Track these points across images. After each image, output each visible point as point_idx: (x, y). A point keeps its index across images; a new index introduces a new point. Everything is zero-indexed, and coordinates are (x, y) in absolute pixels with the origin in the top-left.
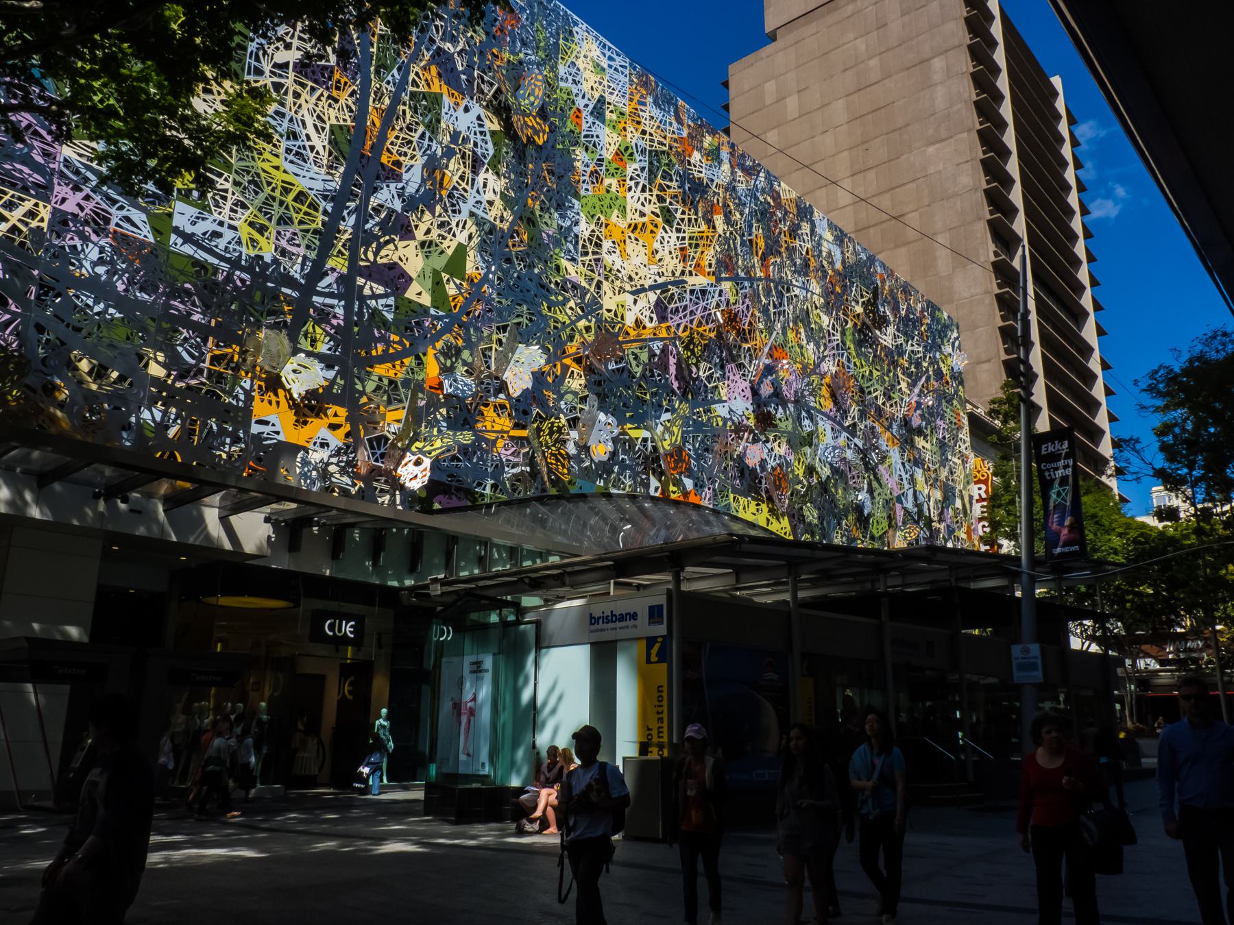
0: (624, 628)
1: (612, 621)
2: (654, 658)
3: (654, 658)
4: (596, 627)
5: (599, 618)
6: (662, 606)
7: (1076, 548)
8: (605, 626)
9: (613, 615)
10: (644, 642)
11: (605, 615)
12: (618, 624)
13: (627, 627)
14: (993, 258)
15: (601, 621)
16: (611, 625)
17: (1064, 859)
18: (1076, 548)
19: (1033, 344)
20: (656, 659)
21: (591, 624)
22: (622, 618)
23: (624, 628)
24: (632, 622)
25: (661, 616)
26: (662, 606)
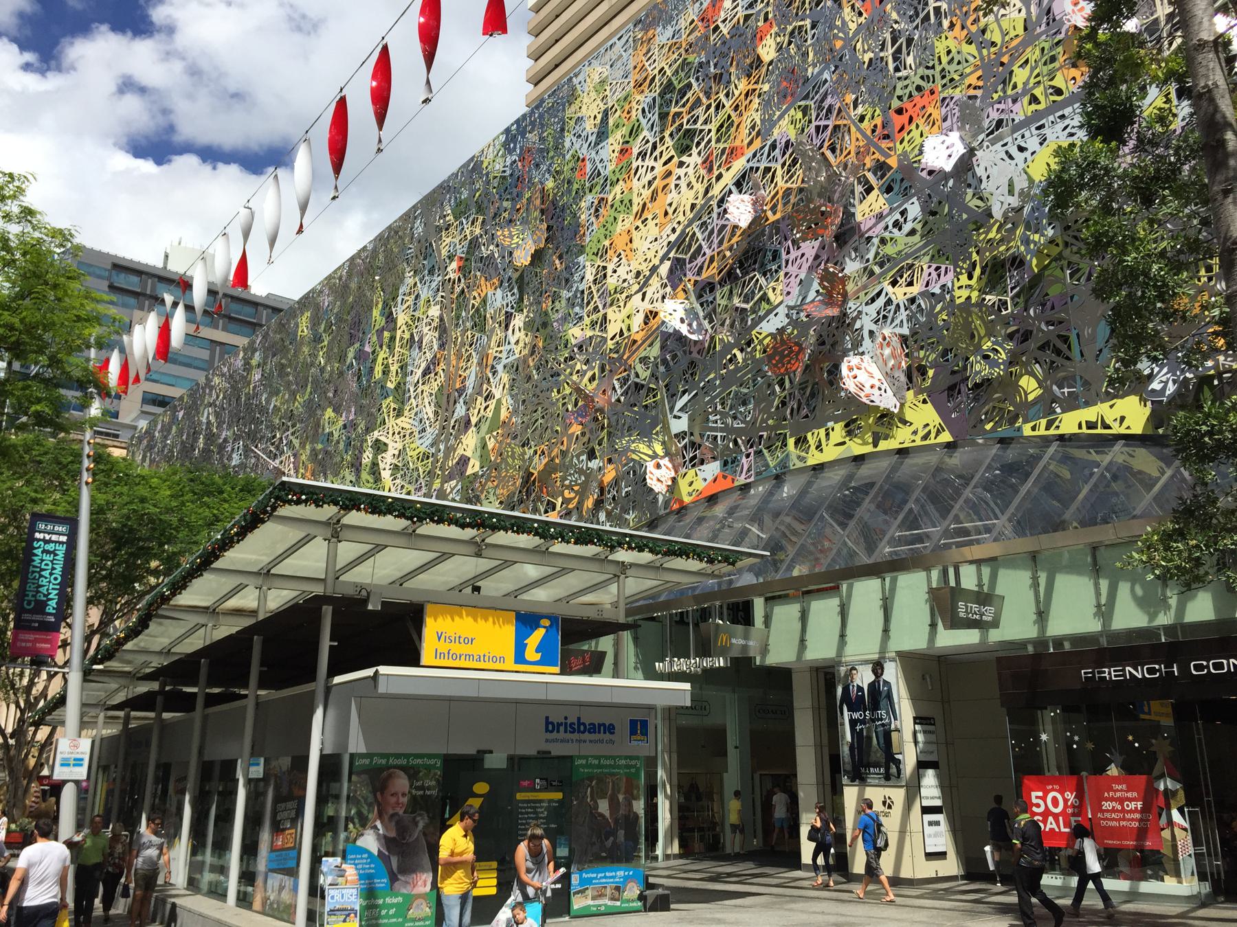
0: (596, 742)
1: (579, 731)
2: (531, 654)
3: (531, 654)
4: (555, 735)
5: (559, 725)
6: (413, 659)
7: (1061, 818)
8: (569, 736)
9: (580, 723)
10: (323, 577)
11: (569, 722)
12: (587, 736)
13: (601, 741)
14: (31, 198)
15: (562, 729)
16: (576, 736)
17: (179, 714)
18: (1061, 818)
19: (278, 688)
20: (538, 657)
21: (547, 730)
22: (593, 729)
23: (596, 742)
24: (607, 736)
25: (469, 501)
26: (413, 659)
